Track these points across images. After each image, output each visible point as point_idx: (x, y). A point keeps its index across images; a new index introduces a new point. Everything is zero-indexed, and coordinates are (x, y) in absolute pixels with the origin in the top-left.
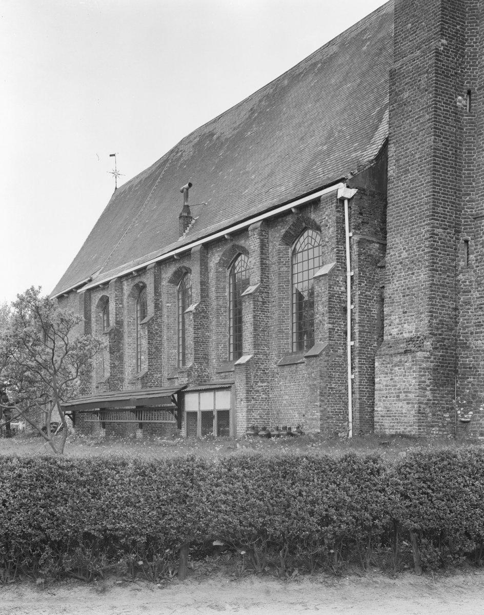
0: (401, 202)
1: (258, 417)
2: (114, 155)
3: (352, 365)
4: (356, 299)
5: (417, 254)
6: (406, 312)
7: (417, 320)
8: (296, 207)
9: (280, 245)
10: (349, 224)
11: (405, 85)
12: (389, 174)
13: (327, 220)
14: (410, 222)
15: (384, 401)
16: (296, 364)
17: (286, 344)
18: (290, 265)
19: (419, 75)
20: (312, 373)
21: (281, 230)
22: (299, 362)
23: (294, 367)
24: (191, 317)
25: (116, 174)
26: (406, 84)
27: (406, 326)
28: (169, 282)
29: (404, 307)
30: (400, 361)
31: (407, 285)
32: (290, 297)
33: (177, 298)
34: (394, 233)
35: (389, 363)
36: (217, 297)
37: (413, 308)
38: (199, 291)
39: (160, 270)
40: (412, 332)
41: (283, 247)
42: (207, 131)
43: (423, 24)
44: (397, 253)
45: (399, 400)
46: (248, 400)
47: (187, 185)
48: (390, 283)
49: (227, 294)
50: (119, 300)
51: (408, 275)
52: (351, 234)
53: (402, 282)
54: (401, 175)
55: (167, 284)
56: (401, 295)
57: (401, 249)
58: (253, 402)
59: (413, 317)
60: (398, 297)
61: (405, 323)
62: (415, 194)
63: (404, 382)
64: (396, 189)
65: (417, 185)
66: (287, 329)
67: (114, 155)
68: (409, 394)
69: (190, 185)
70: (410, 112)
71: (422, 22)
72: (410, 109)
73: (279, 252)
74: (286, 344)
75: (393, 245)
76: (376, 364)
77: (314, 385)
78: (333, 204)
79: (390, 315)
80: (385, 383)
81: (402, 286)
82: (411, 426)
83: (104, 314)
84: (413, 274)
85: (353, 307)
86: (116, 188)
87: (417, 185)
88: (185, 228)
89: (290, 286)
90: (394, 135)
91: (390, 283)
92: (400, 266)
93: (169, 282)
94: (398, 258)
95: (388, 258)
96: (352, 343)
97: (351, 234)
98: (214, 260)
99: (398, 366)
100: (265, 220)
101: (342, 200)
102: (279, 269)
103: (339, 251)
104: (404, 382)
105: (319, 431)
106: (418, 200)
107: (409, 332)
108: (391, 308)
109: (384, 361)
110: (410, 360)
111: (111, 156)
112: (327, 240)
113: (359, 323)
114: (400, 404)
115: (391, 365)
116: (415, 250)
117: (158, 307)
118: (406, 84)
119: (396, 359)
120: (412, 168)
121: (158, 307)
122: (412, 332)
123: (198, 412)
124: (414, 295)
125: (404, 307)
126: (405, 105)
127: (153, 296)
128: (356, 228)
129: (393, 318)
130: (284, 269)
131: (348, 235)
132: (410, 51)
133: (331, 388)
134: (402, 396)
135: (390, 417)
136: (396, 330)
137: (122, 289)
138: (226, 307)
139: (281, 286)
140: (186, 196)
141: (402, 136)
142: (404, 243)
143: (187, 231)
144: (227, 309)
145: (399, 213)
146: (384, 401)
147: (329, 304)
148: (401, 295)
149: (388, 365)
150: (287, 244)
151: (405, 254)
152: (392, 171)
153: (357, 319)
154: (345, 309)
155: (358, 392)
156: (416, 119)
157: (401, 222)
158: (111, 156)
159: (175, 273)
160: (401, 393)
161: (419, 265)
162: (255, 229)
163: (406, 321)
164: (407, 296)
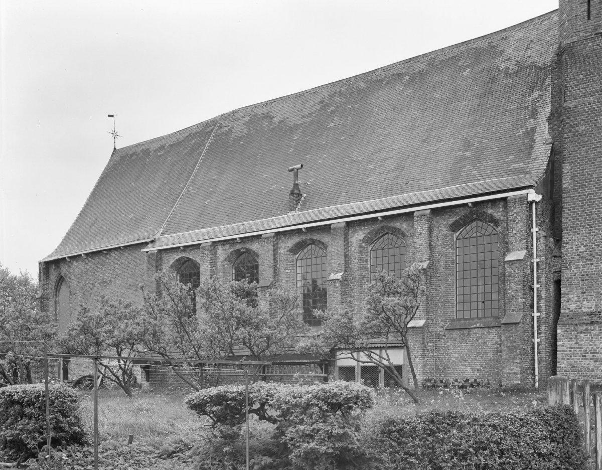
0: (578, 209)
1: (428, 372)
2: (113, 116)
3: (538, 331)
4: (543, 280)
5: (596, 249)
6: (585, 293)
7: (596, 299)
8: (472, 203)
9: (447, 231)
10: (536, 221)
11: (581, 121)
12: (564, 186)
13: (515, 217)
14: (588, 225)
15: (568, 359)
16: (469, 329)
17: (452, 312)
18: (455, 248)
19: (596, 116)
20: (510, 337)
21: (449, 218)
22: (473, 327)
23: (467, 331)
24: (338, 285)
25: (115, 135)
26: (582, 120)
27: (585, 303)
28: (288, 251)
29: (583, 289)
30: (587, 330)
31: (586, 272)
32: (455, 274)
33: (295, 266)
34: (570, 232)
35: (573, 331)
36: (361, 269)
37: (593, 290)
38: (343, 262)
39: (277, 239)
40: (591, 308)
41: (449, 233)
42: (259, 112)
43: (596, 78)
44: (574, 247)
45: (586, 359)
46: (423, 356)
47: (299, 166)
48: (568, 270)
49: (369, 266)
50: (213, 263)
51: (586, 265)
52: (537, 230)
53: (581, 269)
54: (578, 189)
55: (286, 253)
56: (580, 279)
57: (578, 244)
58: (426, 359)
59: (593, 297)
60: (577, 281)
61: (583, 301)
62: (593, 204)
63: (591, 345)
64: (572, 198)
65: (595, 198)
66: (452, 300)
67: (113, 116)
68: (596, 355)
69: (302, 166)
70: (587, 142)
71: (595, 76)
72: (586, 139)
73: (446, 236)
74: (452, 312)
75: (570, 240)
76: (559, 331)
77: (514, 346)
78: (523, 204)
79: (568, 294)
80: (569, 346)
81: (580, 273)
82: (598, 378)
83: (177, 274)
84: (592, 264)
85: (538, 286)
86: (115, 149)
87: (595, 198)
88: (298, 202)
89: (455, 265)
90: (569, 157)
91: (568, 270)
92: (578, 257)
93: (288, 251)
94: (575, 251)
95: (564, 250)
96: (538, 314)
97: (537, 230)
98: (356, 236)
99: (584, 333)
100: (432, 210)
101: (531, 203)
102: (446, 250)
103: (528, 242)
104: (591, 345)
105: (519, 382)
106: (596, 209)
107: (588, 308)
108: (568, 288)
109: (567, 329)
110: (597, 329)
111: (109, 116)
112: (515, 232)
113: (545, 299)
114: (587, 362)
115: (576, 333)
116: (594, 246)
117: (276, 273)
118: (582, 120)
119: (581, 328)
120: (589, 184)
121: (276, 273)
122: (591, 308)
123: (356, 367)
124: (592, 280)
125: (583, 289)
126: (581, 135)
127: (273, 262)
128: (540, 225)
129: (571, 296)
130: (450, 250)
131: (535, 230)
132: (582, 96)
133: (525, 349)
134: (589, 356)
135: (576, 371)
136: (574, 305)
137: (216, 253)
138: (368, 278)
139: (448, 264)
140: (296, 175)
141: (578, 158)
142: (581, 240)
143: (299, 207)
144: (369, 279)
145: (576, 216)
146: (568, 359)
147: (523, 283)
148: (580, 279)
149: (573, 332)
150: (453, 231)
151: (582, 249)
152: (566, 183)
153: (543, 296)
154: (532, 289)
155: (544, 352)
156: (593, 148)
157: (578, 224)
158: (109, 116)
159: (298, 243)
160: (587, 353)
161: (598, 258)
162: (421, 216)
163: (585, 300)
164: (586, 280)
